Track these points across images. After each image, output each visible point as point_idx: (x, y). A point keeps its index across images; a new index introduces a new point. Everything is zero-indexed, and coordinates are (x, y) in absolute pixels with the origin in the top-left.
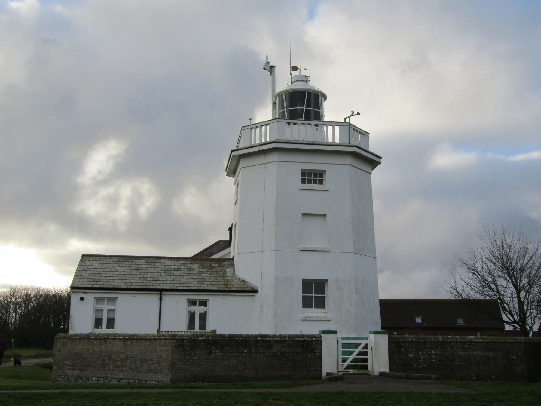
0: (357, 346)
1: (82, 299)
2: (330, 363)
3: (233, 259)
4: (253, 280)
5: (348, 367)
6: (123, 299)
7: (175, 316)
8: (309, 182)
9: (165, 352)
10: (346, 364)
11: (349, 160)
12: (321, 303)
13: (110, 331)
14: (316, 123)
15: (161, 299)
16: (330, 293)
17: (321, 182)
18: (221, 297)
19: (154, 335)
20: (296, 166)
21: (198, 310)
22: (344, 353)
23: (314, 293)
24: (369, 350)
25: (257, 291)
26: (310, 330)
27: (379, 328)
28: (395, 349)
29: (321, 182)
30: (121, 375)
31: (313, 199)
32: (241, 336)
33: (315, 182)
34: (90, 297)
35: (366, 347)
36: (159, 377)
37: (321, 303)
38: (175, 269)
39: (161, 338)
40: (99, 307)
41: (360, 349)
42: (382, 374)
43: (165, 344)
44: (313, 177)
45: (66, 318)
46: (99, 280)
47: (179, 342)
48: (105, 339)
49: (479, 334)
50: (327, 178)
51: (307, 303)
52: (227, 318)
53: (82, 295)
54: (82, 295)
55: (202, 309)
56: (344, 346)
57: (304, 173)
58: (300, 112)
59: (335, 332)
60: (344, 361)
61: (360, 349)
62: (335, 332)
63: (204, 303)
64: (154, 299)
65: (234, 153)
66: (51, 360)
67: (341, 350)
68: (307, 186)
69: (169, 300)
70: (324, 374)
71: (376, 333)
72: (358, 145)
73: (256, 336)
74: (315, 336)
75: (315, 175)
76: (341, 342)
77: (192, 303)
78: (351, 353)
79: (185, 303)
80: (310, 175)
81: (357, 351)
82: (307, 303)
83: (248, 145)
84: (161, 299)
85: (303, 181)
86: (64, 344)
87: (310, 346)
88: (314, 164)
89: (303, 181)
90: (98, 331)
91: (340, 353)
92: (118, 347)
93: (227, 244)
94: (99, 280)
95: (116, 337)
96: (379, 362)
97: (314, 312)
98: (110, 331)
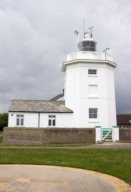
0: (108, 131)
1: (12, 115)
2: (99, 137)
3: (64, 101)
4: (72, 109)
5: (105, 139)
6: (26, 116)
7: (44, 122)
8: (91, 74)
9: (40, 134)
10: (104, 138)
11: (105, 66)
12: (95, 116)
13: (54, 127)
14: (93, 52)
15: (39, 115)
16: (99, 113)
17: (95, 74)
18: (60, 115)
19: (37, 128)
20: (85, 69)
21: (52, 119)
22: (103, 134)
23: (93, 113)
24: (112, 133)
25: (73, 112)
26: (92, 126)
27: (116, 125)
28: (121, 133)
29: (95, 74)
30: (26, 141)
31: (92, 79)
32: (67, 128)
33: (93, 74)
34: (15, 115)
35: (111, 132)
36: (38, 142)
37: (95, 116)
38: (44, 105)
39: (39, 129)
40: (18, 118)
41: (109, 132)
42: (117, 141)
43: (41, 131)
44: (92, 72)
45: (7, 120)
46: (18, 109)
47: (46, 131)
48: (20, 129)
49: (122, 126)
50: (97, 72)
51: (91, 117)
52: (63, 122)
53: (12, 114)
54: (12, 114)
55: (54, 118)
56: (103, 132)
57: (89, 71)
58: (7, 125)
59: (101, 127)
60: (103, 137)
61: (109, 132)
62: (101, 127)
63: (54, 117)
64: (37, 115)
65: (64, 64)
66: (2, 135)
67: (102, 133)
68: (90, 75)
69: (41, 115)
70: (96, 142)
71: (115, 127)
72: (108, 60)
73: (73, 128)
74: (93, 128)
75: (93, 71)
76: (102, 130)
77: (50, 116)
78: (106, 134)
79: (48, 116)
80: (91, 71)
81: (108, 133)
82: (91, 117)
83: (70, 60)
84: (39, 115)
85: (89, 73)
86: (7, 131)
87: (91, 131)
88: (93, 67)
89: (89, 73)
90: (50, 126)
91: (102, 134)
92: (24, 132)
93: (63, 95)
94: (18, 109)
95: (24, 129)
96: (116, 136)
97: (93, 120)
98: (54, 127)
